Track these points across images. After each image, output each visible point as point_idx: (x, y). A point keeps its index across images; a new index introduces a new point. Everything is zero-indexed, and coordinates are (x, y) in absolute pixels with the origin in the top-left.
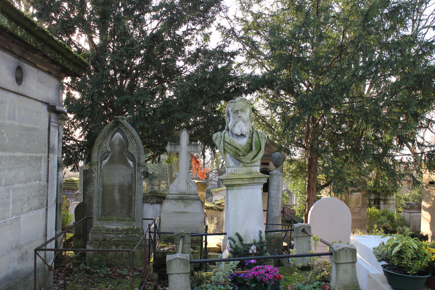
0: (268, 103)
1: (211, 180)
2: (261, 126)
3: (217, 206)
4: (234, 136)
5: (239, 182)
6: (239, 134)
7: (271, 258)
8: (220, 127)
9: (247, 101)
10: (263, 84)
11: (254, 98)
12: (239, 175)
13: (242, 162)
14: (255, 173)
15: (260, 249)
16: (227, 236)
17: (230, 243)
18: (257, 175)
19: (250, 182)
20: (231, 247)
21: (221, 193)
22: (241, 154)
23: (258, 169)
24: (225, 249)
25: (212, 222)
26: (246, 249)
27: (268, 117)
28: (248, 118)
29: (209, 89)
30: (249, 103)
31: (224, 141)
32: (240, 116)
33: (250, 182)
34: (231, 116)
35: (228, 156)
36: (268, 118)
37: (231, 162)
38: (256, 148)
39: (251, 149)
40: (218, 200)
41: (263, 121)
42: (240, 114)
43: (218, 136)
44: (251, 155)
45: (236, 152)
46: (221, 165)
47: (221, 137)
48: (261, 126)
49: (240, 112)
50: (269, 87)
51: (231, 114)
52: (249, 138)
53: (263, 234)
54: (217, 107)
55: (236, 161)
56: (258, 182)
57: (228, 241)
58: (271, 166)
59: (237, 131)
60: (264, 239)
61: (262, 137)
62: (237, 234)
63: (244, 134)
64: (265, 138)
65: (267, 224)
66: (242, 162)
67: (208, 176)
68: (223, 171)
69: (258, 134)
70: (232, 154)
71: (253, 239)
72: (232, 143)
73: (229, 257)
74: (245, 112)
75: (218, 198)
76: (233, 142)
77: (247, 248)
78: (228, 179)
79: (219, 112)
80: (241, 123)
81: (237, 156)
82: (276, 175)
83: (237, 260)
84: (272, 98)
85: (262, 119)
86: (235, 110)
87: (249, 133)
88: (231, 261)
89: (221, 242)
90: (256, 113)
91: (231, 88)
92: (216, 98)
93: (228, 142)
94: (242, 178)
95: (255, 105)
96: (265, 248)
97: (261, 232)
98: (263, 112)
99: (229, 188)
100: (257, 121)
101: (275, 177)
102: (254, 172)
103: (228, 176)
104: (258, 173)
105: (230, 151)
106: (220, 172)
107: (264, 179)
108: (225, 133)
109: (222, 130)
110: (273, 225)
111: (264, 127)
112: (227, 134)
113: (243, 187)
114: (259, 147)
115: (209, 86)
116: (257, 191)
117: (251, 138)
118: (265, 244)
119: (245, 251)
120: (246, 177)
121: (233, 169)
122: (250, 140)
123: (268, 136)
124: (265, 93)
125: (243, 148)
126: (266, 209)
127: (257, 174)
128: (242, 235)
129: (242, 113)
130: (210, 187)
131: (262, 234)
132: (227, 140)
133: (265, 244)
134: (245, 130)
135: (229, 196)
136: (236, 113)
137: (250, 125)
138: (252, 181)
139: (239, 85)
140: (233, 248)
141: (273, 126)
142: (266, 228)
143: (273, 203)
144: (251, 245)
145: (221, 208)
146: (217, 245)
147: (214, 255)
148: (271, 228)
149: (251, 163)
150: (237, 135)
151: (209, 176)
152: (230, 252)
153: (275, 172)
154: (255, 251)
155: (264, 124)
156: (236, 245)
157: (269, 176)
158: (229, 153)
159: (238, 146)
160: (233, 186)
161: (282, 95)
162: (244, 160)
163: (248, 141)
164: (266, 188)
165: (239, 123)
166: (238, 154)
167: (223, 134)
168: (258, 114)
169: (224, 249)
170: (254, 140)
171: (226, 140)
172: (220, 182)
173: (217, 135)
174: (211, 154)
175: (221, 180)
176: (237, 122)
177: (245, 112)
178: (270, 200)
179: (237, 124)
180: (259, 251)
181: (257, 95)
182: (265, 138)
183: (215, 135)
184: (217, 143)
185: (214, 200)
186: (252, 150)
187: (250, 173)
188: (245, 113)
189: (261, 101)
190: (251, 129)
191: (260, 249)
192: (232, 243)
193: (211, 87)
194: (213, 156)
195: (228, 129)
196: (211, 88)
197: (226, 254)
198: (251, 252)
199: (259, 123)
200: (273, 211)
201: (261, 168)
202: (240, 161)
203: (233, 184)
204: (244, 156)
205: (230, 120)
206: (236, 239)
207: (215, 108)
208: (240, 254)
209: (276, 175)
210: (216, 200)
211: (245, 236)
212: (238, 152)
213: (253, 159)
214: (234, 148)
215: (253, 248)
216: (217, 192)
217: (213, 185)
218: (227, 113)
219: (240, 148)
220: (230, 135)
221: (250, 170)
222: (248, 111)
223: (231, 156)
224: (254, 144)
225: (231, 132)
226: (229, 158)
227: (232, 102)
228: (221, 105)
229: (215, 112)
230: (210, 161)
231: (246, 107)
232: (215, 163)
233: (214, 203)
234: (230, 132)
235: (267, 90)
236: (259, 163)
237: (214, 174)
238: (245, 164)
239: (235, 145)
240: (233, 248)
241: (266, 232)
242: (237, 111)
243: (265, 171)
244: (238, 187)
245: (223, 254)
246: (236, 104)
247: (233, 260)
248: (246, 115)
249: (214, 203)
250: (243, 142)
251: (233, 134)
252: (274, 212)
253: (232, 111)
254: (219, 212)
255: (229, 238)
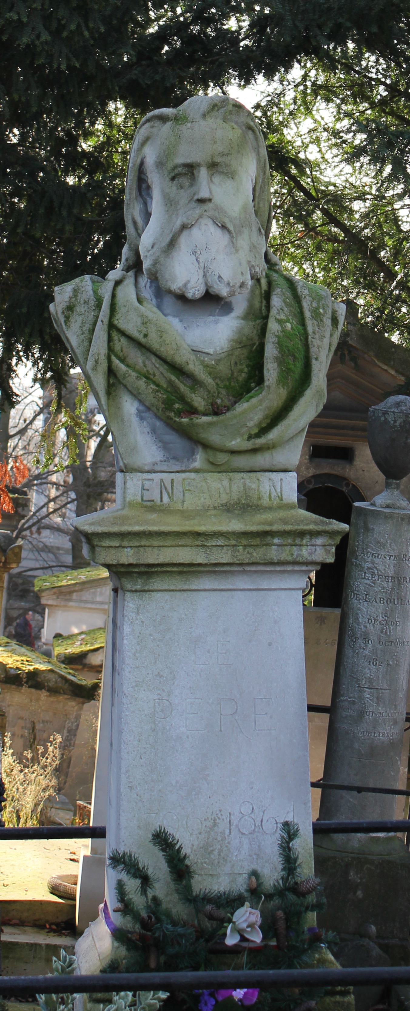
0: (362, 127)
1: (40, 525)
2: (319, 248)
3: (64, 670)
4: (169, 302)
5: (184, 555)
6: (195, 290)
7: (344, 981)
8: (100, 242)
9: (243, 119)
10: (339, 26)
11: (290, 95)
12: (185, 514)
13: (206, 446)
14: (270, 509)
15: (281, 925)
16: (109, 845)
17: (120, 887)
18: (284, 521)
19: (242, 555)
20: (126, 907)
21: (86, 595)
22: (198, 400)
23: (288, 487)
24: (94, 917)
25: (35, 760)
26: (208, 925)
27: (361, 197)
28: (245, 208)
29: (45, 37)
30: (264, 127)
31: (112, 326)
32: (204, 194)
33: (242, 555)
34: (156, 193)
35: (129, 407)
36: (357, 206)
37: (142, 442)
38: (283, 379)
39: (256, 376)
40: (71, 637)
41: (331, 219)
42: (205, 185)
43: (82, 297)
44: (253, 410)
45: (174, 390)
46: (93, 444)
47: (99, 306)
48: (319, 248)
49: (203, 173)
50: (368, 43)
51: (156, 180)
52: (249, 315)
53: (304, 844)
54: (88, 135)
55: (172, 437)
56: (285, 556)
57: (110, 877)
58: (365, 466)
59: (185, 273)
60: (307, 869)
61: (317, 315)
62: (162, 840)
63: (224, 292)
64: (335, 321)
65: (327, 786)
66: (206, 446)
67: (21, 504)
68: (103, 475)
69: (297, 298)
70: (150, 399)
71: (247, 867)
72: (154, 341)
73: (113, 967)
74: (231, 174)
75: (71, 626)
76: (161, 333)
77: (211, 917)
78: (122, 535)
79: (95, 163)
80: (206, 234)
81: (179, 413)
82: (388, 517)
83: (156, 987)
84: (384, 102)
85: (325, 212)
86: (180, 160)
87: (246, 292)
88: (119, 988)
89: (77, 870)
90: (293, 178)
91: (163, 36)
92: (85, 92)
93: (135, 334)
94: (198, 534)
95: (289, 133)
96: (312, 918)
97: (290, 832)
98: (335, 173)
99: (128, 585)
100: (300, 219)
101: (381, 530)
102: (265, 502)
103: (124, 519)
104: (290, 507)
105: (142, 383)
106: (90, 488)
107: (320, 541)
108: (118, 283)
109: (100, 266)
110: (359, 790)
111: (336, 252)
112: (128, 292)
113: (206, 583)
114: (298, 368)
115: (47, 18)
116: (281, 608)
117: (260, 315)
118: (312, 899)
119: (201, 933)
120: (224, 528)
121: (156, 482)
122: (250, 329)
123: (351, 306)
124: (348, 68)
125: (211, 370)
126: (328, 703)
127: (282, 514)
128: (188, 842)
129: (217, 179)
130: (28, 561)
131: (296, 844)
132: (129, 323)
133: (312, 899)
134: (227, 275)
135: (127, 629)
136: (185, 181)
137: (253, 248)
138: (252, 550)
139: (208, 21)
140: (136, 916)
141: (383, 246)
142: (326, 807)
143: (369, 671)
144: (233, 902)
145: (85, 680)
146: (54, 890)
147: (34, 946)
148: (349, 810)
149: (254, 451)
150: (182, 298)
151: (25, 504)
152: (119, 935)
153: (381, 499)
154: (257, 938)
155: (333, 239)
156: (155, 899)
157: (345, 527)
158: (136, 395)
159: (183, 357)
160: (149, 571)
161: (357, 254)
162: (214, 437)
163: (240, 331)
164: (331, 588)
165: (195, 231)
166: (182, 399)
167: (106, 290)
168: (306, 182)
169: (90, 916)
170: (273, 326)
171: (121, 322)
172: (85, 544)
173: (76, 292)
174: (43, 383)
175: (89, 537)
176: (184, 227)
177: (231, 174)
178: (348, 651)
179: (183, 240)
180: (276, 935)
181: (305, 77)
182: (335, 321)
183: (63, 293)
184: (73, 336)
185: (46, 634)
186: (260, 381)
187: (245, 506)
188: (229, 184)
189: (325, 112)
190: (261, 267)
191: (281, 925)
192: (132, 885)
193: (61, 28)
194: (55, 393)
195: (136, 265)
196: (56, 34)
197: (95, 949)
198: (231, 940)
199: (310, 230)
200: (361, 714)
201: (311, 472)
202: (194, 440)
203: (151, 560)
204: (216, 411)
205: (147, 215)
206: (155, 863)
207: (73, 141)
208: (171, 951)
209: (388, 517)
210: (58, 636)
211: (207, 849)
212: (182, 388)
213: (264, 430)
214: (163, 368)
215: (247, 917)
216: (64, 593)
217: (47, 549)
218: (132, 175)
219: (195, 367)
220: (147, 293)
221: (246, 489)
222: (249, 168)
223: (146, 408)
224: (270, 351)
225: (154, 278)
226: (135, 420)
227: (163, 119)
228: (110, 125)
229: (75, 161)
230: (39, 423)
231: (240, 146)
232: (62, 434)
233: (48, 654)
234: (144, 281)
235: (359, 56)
236: (294, 453)
237: (53, 493)
238: (222, 458)
239: (167, 351)
240: (136, 916)
241: (319, 830)
242: (190, 169)
243: (327, 496)
244: (177, 583)
245: (83, 944)
246: (185, 129)
247: (135, 988)
248: (234, 194)
249: (48, 654)
250: (216, 335)
251: (161, 293)
252: (369, 717)
253: (160, 164)
254: (72, 705)
255: (117, 860)
